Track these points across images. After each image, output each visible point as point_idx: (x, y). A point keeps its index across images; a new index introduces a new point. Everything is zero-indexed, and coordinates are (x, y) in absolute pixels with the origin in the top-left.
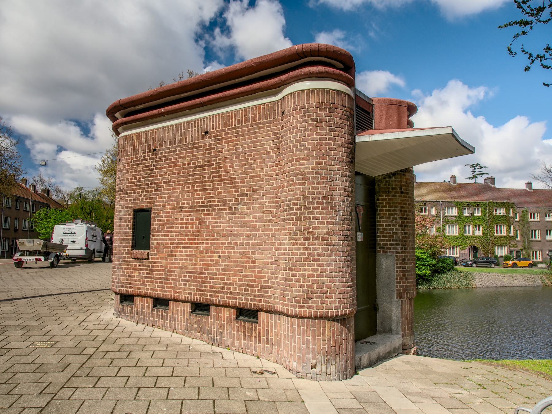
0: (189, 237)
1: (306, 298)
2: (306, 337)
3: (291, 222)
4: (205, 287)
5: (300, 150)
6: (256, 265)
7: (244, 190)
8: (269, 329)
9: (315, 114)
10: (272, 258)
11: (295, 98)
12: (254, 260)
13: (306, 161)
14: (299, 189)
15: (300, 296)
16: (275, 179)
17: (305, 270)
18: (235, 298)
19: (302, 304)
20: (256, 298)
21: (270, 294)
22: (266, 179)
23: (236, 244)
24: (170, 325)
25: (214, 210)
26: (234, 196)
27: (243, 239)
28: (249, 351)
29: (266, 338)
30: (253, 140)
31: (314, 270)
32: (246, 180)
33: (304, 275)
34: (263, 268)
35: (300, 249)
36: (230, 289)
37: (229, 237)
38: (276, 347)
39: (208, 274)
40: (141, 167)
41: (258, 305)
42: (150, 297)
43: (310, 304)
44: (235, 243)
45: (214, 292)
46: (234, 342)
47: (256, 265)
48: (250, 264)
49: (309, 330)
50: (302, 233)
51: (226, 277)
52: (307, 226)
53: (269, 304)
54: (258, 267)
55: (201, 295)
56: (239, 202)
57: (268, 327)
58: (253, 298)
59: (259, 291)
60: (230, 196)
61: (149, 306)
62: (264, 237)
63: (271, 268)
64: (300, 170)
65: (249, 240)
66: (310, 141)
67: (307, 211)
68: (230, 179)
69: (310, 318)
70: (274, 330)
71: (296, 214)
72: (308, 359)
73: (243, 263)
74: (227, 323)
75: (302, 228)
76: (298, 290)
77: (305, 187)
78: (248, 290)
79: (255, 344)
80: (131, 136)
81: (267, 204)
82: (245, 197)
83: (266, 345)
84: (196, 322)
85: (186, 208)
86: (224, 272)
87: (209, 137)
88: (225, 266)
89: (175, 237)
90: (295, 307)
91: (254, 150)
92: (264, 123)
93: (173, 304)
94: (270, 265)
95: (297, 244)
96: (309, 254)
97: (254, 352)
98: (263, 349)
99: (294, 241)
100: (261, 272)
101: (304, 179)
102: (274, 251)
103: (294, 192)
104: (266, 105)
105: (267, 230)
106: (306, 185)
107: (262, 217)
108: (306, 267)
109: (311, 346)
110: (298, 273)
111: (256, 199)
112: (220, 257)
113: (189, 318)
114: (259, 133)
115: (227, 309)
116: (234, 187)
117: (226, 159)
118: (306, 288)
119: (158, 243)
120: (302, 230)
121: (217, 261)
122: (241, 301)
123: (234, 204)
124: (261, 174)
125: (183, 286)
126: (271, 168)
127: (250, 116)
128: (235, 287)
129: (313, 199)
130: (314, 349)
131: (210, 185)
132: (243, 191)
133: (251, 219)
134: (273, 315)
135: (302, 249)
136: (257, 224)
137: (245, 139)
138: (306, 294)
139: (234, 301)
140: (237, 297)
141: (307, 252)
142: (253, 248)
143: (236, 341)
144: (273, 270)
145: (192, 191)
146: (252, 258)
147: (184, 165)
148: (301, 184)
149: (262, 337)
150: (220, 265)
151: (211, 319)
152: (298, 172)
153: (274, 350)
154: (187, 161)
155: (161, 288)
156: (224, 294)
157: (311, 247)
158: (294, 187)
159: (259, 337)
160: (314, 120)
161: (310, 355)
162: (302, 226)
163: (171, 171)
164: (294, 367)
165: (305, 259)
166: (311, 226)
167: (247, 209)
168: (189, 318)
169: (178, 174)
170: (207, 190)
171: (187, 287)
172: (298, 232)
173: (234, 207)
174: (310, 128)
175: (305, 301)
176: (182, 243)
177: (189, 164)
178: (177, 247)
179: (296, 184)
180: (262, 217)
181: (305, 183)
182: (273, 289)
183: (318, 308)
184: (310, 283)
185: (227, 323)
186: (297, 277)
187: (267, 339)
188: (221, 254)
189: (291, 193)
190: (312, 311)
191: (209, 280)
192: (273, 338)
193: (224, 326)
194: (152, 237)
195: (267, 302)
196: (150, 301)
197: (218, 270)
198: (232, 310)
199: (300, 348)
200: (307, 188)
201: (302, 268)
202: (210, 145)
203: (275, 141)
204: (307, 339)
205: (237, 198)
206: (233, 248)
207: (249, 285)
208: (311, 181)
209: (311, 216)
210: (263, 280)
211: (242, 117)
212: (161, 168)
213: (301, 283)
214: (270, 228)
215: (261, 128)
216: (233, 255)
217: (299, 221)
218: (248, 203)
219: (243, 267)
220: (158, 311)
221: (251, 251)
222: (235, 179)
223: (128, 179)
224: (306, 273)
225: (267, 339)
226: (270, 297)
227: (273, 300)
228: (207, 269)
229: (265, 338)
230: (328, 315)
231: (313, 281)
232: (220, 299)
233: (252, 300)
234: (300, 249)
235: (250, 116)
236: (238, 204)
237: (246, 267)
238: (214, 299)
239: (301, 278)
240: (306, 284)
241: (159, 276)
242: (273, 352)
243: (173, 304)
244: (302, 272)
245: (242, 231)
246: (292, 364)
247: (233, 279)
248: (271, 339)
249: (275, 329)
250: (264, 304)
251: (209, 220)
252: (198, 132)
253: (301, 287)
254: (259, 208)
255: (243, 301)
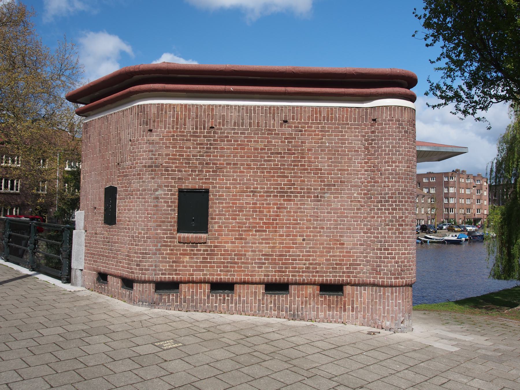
0: (265, 221)
1: (400, 271)
2: (398, 301)
3: (387, 211)
4: (286, 268)
5: (396, 154)
6: (345, 246)
7: (331, 181)
8: (355, 299)
9: (406, 127)
10: (361, 240)
11: (390, 111)
12: (342, 242)
13: (400, 164)
14: (395, 186)
15: (395, 270)
16: (363, 174)
17: (399, 250)
18: (323, 276)
19: (397, 276)
20: (345, 275)
21: (358, 270)
22: (354, 173)
23: (323, 228)
24: (236, 308)
25: (296, 196)
26: (320, 185)
27: (331, 224)
28: (335, 320)
29: (352, 307)
30: (340, 137)
31: (406, 249)
32: (333, 172)
33: (398, 254)
34: (351, 249)
35: (395, 233)
36: (316, 268)
37: (315, 222)
38: (362, 313)
39: (290, 256)
40: (191, 144)
41: (347, 280)
42: (205, 282)
43: (403, 276)
44: (322, 227)
45: (298, 272)
46: (317, 315)
47: (345, 246)
48: (338, 246)
49: (400, 295)
50: (397, 221)
51: (311, 258)
52: (401, 215)
53: (358, 279)
54: (347, 248)
55: (282, 276)
56: (326, 191)
57: (353, 297)
58: (341, 274)
59: (347, 268)
60: (315, 185)
61: (204, 291)
62: (352, 222)
63: (360, 249)
64: (395, 170)
65: (337, 225)
66: (403, 149)
67: (401, 204)
68: (315, 170)
69: (402, 286)
70: (359, 299)
71: (392, 205)
72: (400, 318)
73: (330, 245)
74: (310, 299)
75: (398, 217)
76: (394, 265)
77: (400, 185)
78: (336, 268)
79: (341, 313)
80: (174, 106)
81: (355, 195)
82: (333, 188)
83: (351, 313)
84: (271, 302)
85: (260, 192)
86: (309, 254)
87: (289, 127)
88: (310, 248)
89: (244, 221)
90: (391, 278)
91: (342, 147)
92: (351, 125)
93: (137, 286)
94: (359, 246)
95: (393, 230)
96: (403, 237)
97: (339, 320)
98: (348, 316)
99: (390, 227)
100: (350, 252)
101: (399, 178)
102: (362, 234)
103: (390, 187)
104: (354, 109)
105: (356, 217)
106: (401, 183)
107: (351, 205)
108: (400, 247)
109: (401, 308)
110: (393, 252)
111: (344, 190)
112: (304, 240)
113: (263, 299)
114: (346, 132)
115: (310, 286)
116: (319, 177)
117: (309, 150)
118: (400, 264)
119: (219, 227)
120: (398, 218)
121: (301, 244)
122: (329, 278)
123: (319, 193)
124: (349, 168)
125: (257, 269)
126: (360, 165)
127: (337, 116)
128: (322, 266)
129: (405, 194)
130: (403, 309)
131: (291, 173)
132: (330, 182)
133: (339, 207)
134: (359, 287)
135: (397, 233)
136: (346, 211)
137: (331, 135)
138: (400, 268)
139: (321, 278)
140: (324, 275)
141: (401, 236)
142: (341, 232)
143: (320, 313)
144: (362, 250)
145: (267, 176)
146: (340, 240)
147: (256, 149)
148: (396, 182)
149: (347, 307)
150: (305, 248)
151: (291, 297)
152: (394, 172)
153: (359, 316)
154: (260, 146)
155: (226, 272)
156: (309, 273)
157: (404, 232)
158: (390, 184)
159: (345, 306)
160: (406, 132)
161: (400, 314)
162: (398, 216)
163: (237, 153)
164: (387, 326)
165: (399, 241)
166: (404, 216)
167: (334, 198)
168: (263, 299)
169: (248, 157)
170: (287, 177)
171: (263, 269)
172: (394, 219)
173: (319, 195)
174: (403, 138)
175: (400, 273)
176: (255, 227)
177: (262, 149)
178: (247, 231)
179: (392, 182)
180: (351, 205)
181: (399, 181)
182: (362, 266)
183: (408, 278)
184: (403, 260)
185: (310, 299)
186: (393, 255)
187: (353, 307)
188: (305, 237)
189: (387, 188)
190: (404, 280)
191: (291, 261)
192: (359, 306)
193: (306, 302)
194: (210, 220)
195: (356, 277)
196: (152, 286)
197: (302, 252)
198: (315, 287)
199: (393, 310)
200: (400, 186)
201: (397, 248)
202: (291, 134)
203: (363, 142)
204: (399, 302)
205: (323, 187)
206: (320, 232)
207: (336, 264)
208: (404, 180)
209: (404, 207)
210: (351, 259)
211: (328, 115)
212: (222, 148)
213: (397, 260)
214: (359, 215)
215: (348, 128)
216: (319, 238)
217: (394, 211)
218: (335, 193)
219: (331, 248)
220: (220, 296)
221: (339, 235)
222: (321, 170)
223: (167, 155)
224: (400, 252)
225: (353, 307)
226: (359, 273)
227: (361, 274)
228: (289, 252)
229: (350, 307)
230: (375, 283)
231: (405, 258)
232: (304, 278)
233: (340, 276)
234: (395, 233)
235: (337, 116)
236: (324, 193)
237: (333, 248)
238: (298, 278)
239: (397, 256)
240: (400, 260)
241: (222, 260)
242: (359, 318)
243: (137, 286)
244: (397, 251)
245: (329, 216)
246: (385, 324)
247: (320, 260)
248: (357, 307)
249: (361, 298)
250: (353, 279)
251: (290, 206)
252: (274, 118)
253: (396, 263)
254: (348, 197)
255: (331, 278)
